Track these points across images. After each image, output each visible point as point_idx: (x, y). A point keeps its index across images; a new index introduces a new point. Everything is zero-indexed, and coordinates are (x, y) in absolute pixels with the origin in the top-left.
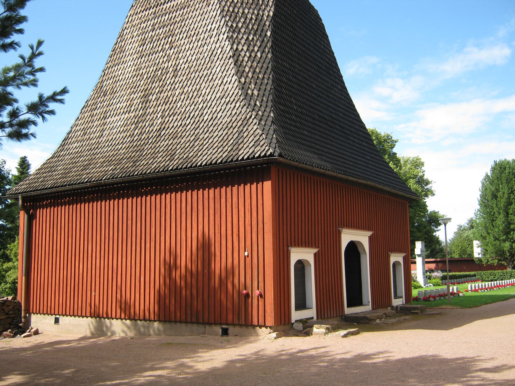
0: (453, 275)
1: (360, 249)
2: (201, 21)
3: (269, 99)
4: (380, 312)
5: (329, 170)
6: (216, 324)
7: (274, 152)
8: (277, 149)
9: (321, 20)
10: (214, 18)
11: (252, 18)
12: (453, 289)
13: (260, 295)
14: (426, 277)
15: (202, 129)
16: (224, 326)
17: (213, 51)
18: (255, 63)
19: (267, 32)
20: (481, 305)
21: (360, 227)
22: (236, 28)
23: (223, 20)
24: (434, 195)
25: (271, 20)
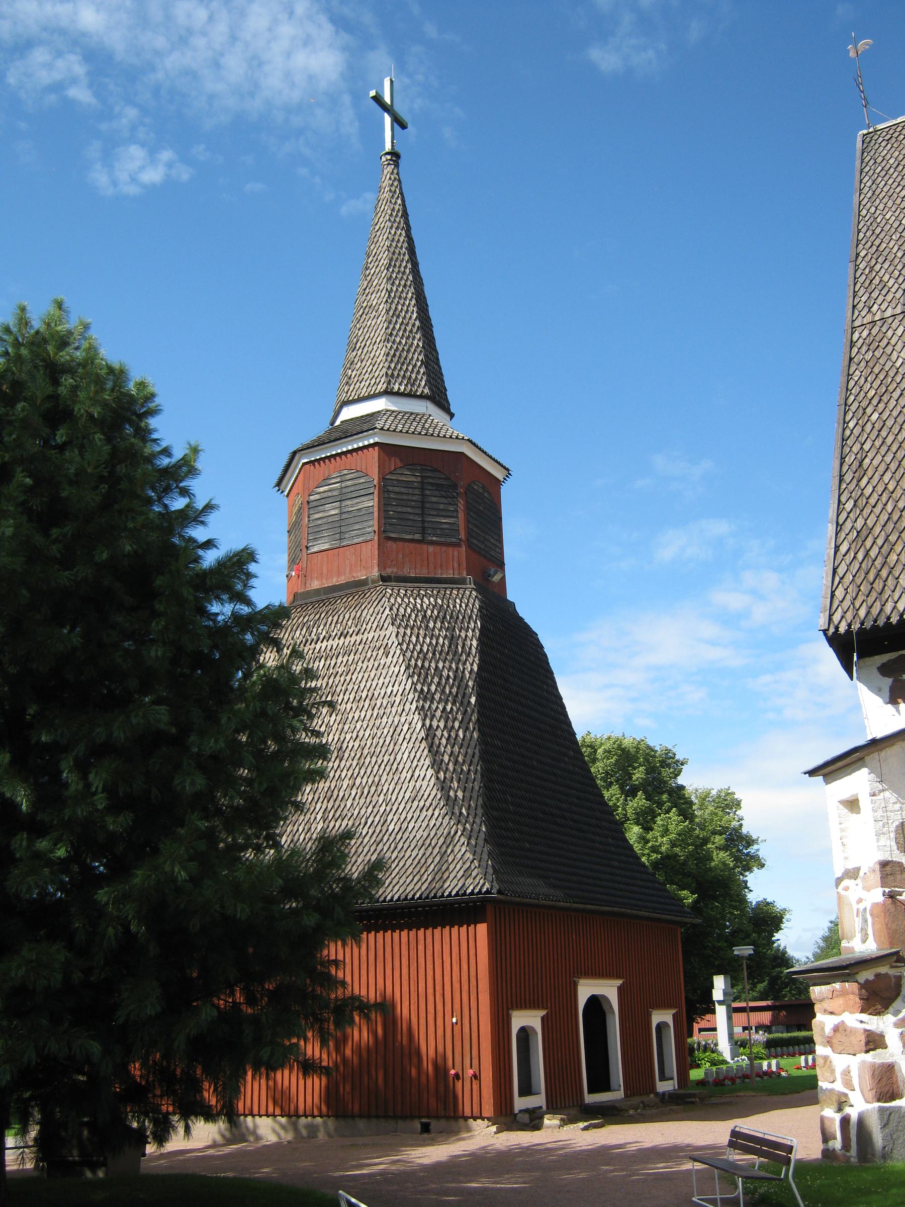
0: (794, 1037)
1: (605, 1007)
2: (376, 678)
3: (479, 804)
4: (636, 1100)
5: (559, 901)
6: (412, 1117)
7: (492, 889)
8: (495, 883)
10: (397, 676)
11: (448, 676)
12: (769, 1065)
13: (475, 1076)
14: (736, 1043)
15: (388, 844)
16: (423, 1120)
18: (456, 747)
19: (470, 697)
20: (803, 1091)
22: (427, 693)
23: (410, 681)
24: (763, 866)
25: (476, 677)
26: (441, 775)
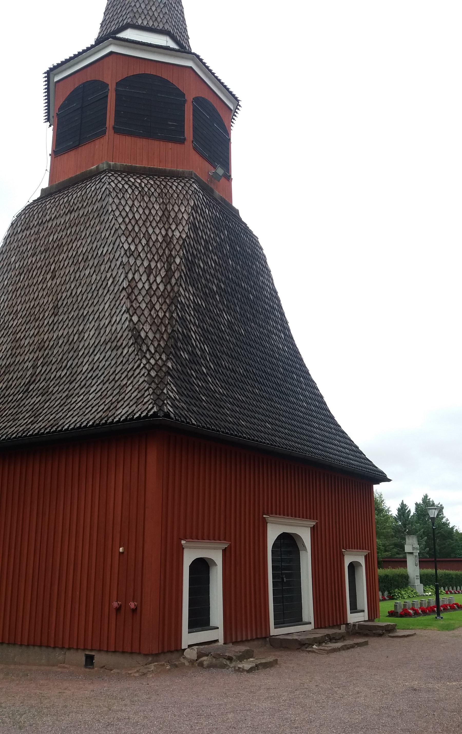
9: (262, 249)
16: (88, 653)
17: (103, 281)
21: (286, 512)
26: (135, 319)
